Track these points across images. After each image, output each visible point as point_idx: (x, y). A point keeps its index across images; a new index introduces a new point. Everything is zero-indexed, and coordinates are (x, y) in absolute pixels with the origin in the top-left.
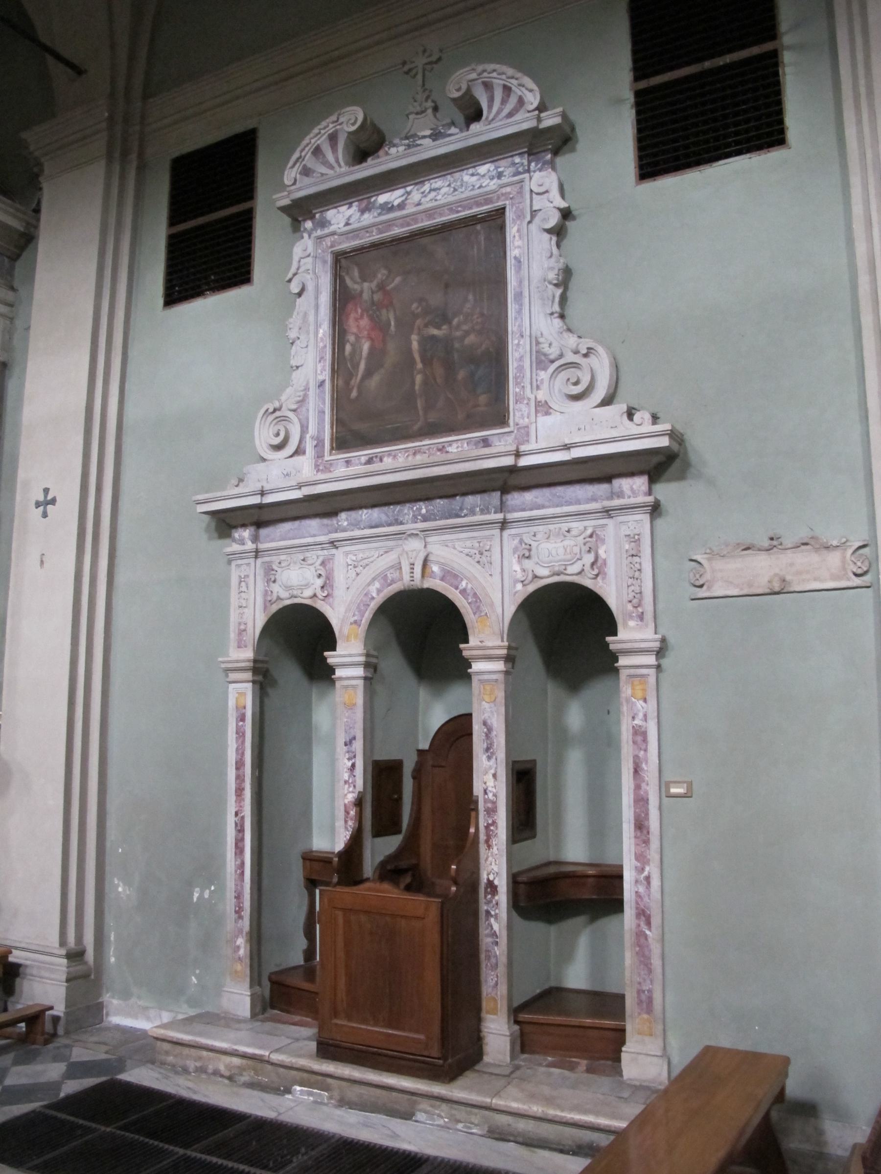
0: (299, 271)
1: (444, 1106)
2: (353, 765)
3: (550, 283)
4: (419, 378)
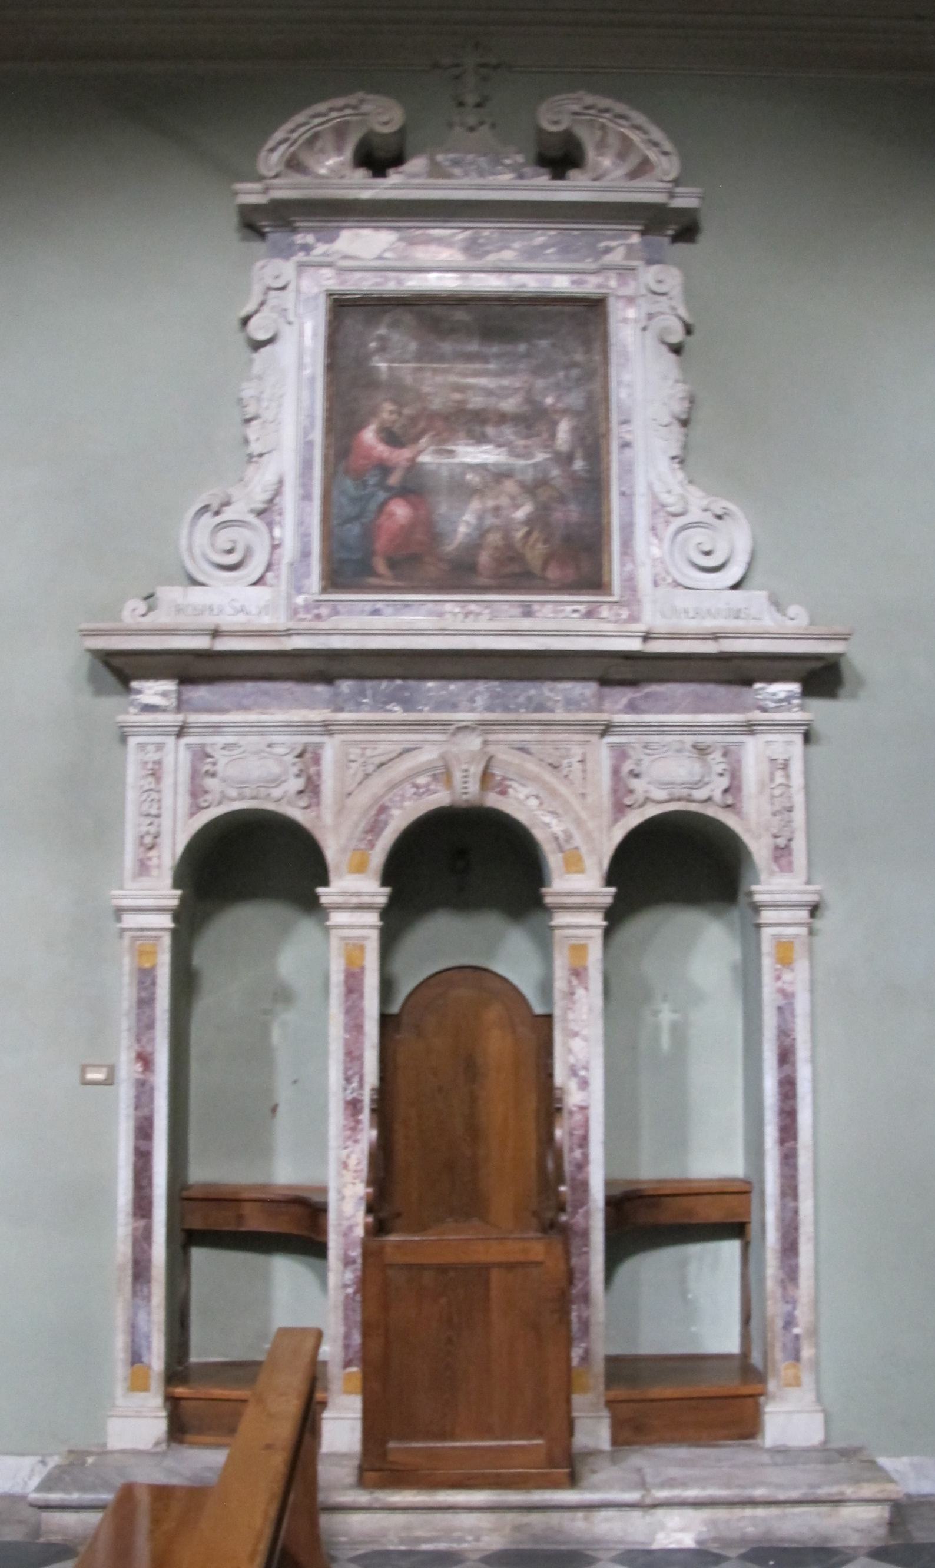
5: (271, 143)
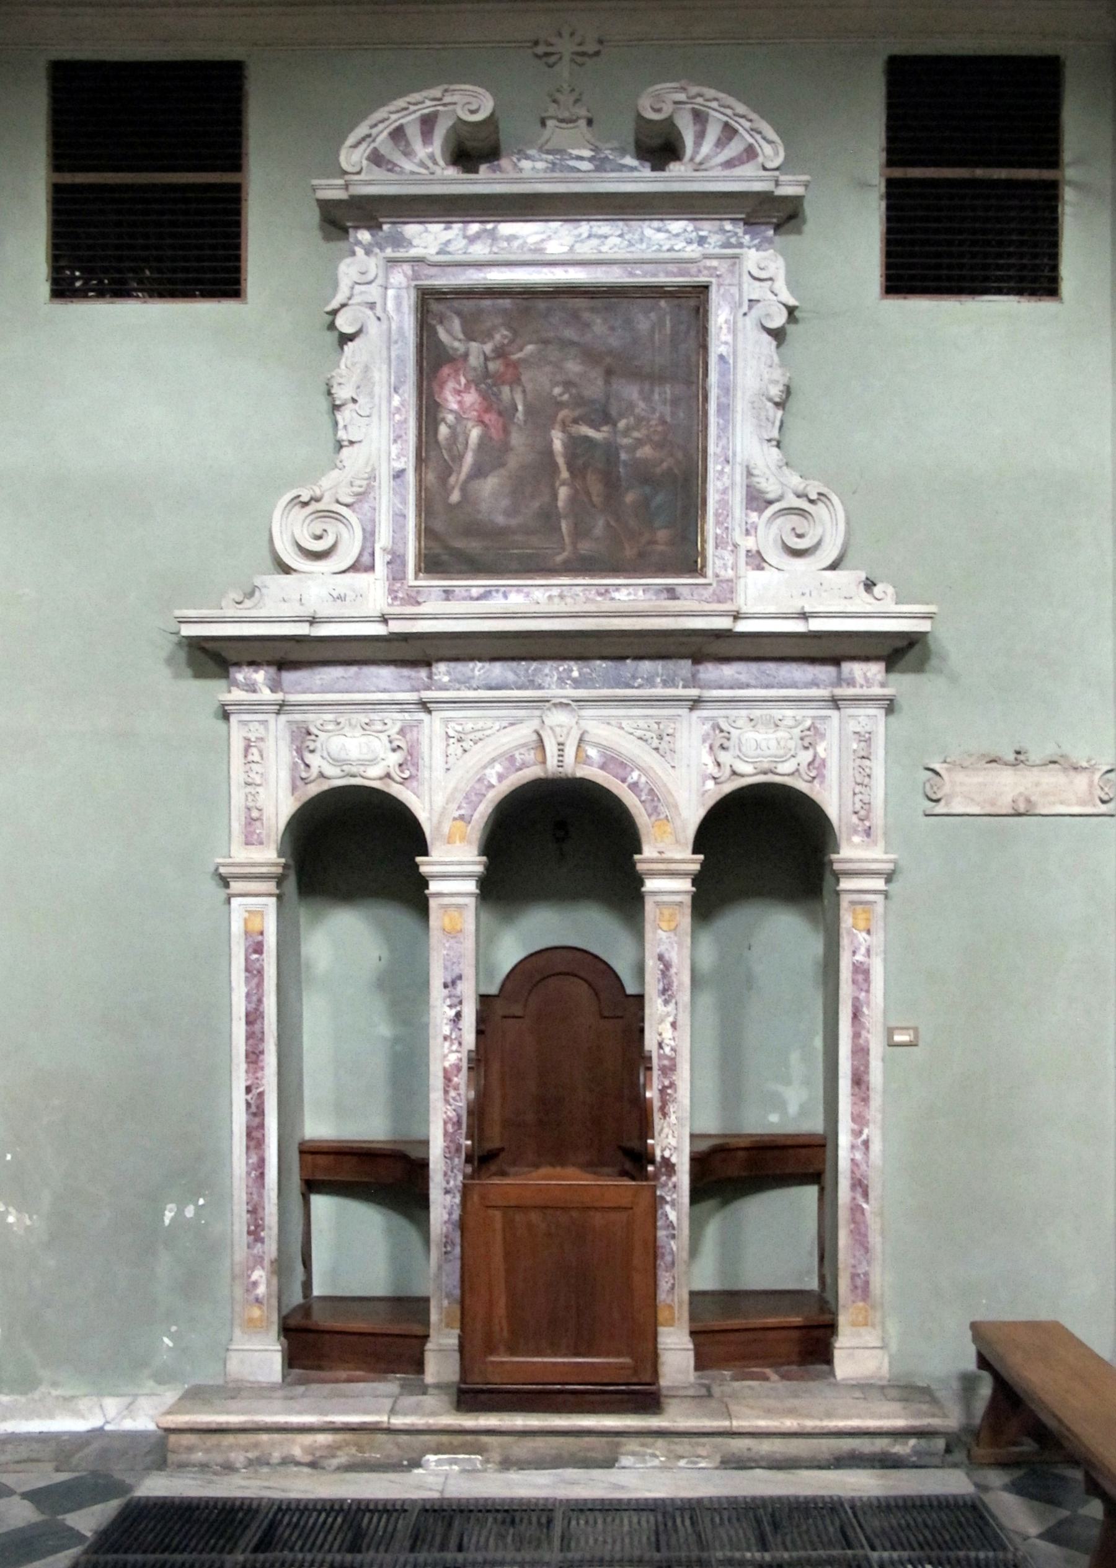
0: (350, 302)
1: (660, 1442)
2: (458, 1015)
3: (770, 400)
4: (563, 492)
5: (351, 139)
